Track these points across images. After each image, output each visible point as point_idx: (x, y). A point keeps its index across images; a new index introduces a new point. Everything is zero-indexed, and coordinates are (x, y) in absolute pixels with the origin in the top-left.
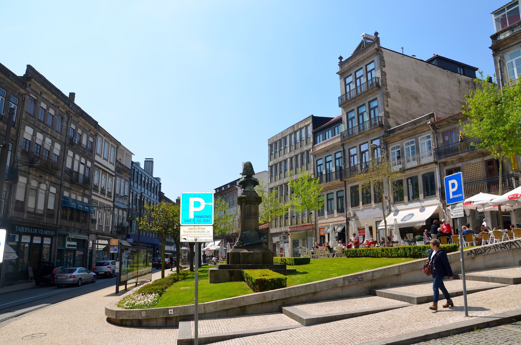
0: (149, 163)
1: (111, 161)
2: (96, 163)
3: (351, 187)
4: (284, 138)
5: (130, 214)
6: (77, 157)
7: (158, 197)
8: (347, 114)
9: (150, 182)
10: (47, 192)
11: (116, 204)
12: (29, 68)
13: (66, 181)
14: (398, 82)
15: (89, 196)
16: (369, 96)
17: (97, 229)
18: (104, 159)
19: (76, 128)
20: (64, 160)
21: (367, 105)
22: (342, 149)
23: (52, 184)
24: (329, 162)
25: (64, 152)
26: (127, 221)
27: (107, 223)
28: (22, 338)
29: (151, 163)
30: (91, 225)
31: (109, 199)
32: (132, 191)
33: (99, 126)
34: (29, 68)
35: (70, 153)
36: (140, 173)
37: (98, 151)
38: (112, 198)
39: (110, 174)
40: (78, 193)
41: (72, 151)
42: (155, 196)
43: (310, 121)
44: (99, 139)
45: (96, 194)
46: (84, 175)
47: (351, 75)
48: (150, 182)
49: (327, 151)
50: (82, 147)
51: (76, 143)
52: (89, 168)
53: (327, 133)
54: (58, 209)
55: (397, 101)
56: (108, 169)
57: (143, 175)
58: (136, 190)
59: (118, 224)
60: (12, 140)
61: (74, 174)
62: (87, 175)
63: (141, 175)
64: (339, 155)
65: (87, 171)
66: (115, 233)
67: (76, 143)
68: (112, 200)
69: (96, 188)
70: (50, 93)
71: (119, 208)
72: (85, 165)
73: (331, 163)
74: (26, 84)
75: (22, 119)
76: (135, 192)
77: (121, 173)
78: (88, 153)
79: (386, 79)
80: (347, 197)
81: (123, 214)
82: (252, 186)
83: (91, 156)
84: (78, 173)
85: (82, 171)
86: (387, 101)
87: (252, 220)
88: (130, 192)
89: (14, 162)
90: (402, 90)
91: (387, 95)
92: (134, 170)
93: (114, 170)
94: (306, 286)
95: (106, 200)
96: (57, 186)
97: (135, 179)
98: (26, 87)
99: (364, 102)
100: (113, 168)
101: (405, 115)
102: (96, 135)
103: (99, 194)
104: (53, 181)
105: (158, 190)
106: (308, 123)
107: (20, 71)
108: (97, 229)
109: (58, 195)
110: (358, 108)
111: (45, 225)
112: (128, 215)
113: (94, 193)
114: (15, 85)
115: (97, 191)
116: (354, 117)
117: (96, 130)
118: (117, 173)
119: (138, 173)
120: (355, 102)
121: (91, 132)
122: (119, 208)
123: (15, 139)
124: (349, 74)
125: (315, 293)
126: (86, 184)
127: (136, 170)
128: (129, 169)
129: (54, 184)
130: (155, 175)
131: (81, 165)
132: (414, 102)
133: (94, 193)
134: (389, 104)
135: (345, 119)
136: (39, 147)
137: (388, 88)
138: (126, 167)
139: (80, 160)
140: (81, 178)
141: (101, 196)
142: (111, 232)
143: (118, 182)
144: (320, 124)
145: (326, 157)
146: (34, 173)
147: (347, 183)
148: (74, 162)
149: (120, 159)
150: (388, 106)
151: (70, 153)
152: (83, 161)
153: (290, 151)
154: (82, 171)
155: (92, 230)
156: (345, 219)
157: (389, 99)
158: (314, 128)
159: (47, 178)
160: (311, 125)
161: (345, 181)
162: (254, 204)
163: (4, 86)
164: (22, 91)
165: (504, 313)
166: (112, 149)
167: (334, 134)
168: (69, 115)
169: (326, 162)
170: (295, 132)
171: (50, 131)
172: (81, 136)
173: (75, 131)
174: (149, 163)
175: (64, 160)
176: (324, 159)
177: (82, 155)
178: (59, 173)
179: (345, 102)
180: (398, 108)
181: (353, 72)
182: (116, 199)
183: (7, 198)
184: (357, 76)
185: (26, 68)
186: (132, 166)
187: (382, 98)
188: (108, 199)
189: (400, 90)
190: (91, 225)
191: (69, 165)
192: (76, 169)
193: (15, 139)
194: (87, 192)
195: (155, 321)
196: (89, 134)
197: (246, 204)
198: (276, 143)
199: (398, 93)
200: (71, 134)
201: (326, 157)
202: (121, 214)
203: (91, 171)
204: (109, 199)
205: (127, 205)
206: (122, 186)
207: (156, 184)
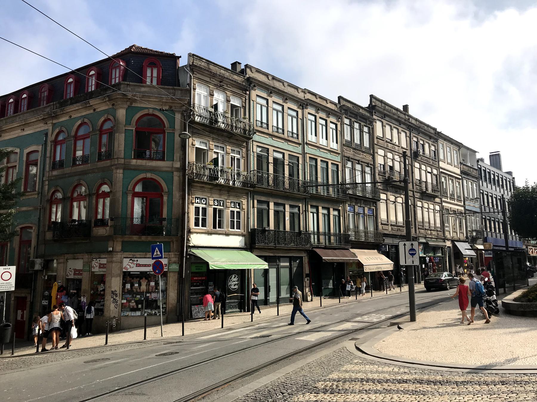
2: (441, 170)
6: (423, 167)
31: (460, 203)
38: (462, 202)
45: (446, 200)
68: (462, 204)
92: (480, 169)
95: (457, 205)
100: (458, 171)
113: (443, 199)
119: (485, 171)
127: (483, 168)
133: (443, 199)
146: (391, 188)
151: (417, 165)
152: (429, 169)
177: (427, 164)
191: (417, 177)
192: (424, 179)
193: (372, 163)
206: (470, 187)
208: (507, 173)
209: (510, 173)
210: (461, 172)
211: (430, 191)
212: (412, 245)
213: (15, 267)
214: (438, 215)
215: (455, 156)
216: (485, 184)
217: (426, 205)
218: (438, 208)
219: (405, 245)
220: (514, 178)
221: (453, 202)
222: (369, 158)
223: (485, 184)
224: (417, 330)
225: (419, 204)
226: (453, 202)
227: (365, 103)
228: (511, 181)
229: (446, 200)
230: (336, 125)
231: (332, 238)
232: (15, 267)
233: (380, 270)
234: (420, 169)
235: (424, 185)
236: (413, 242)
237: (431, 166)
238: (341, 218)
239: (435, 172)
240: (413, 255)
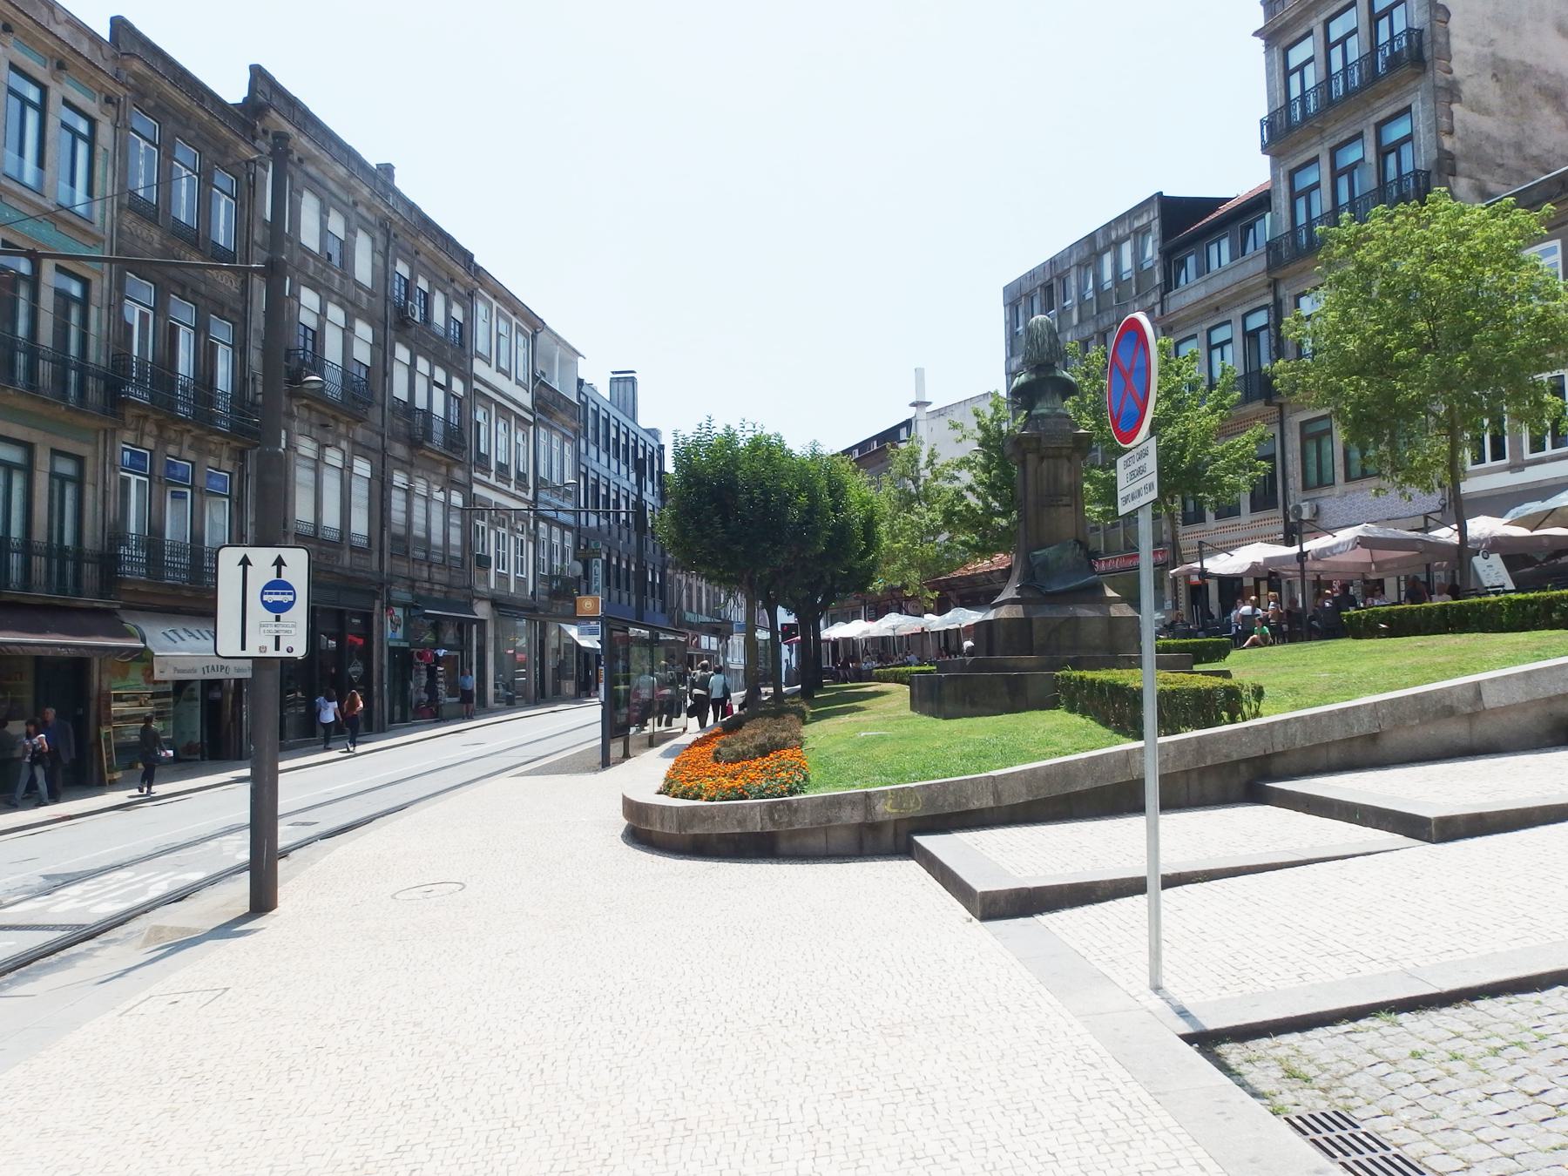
0: (625, 383)
1: (521, 377)
2: (476, 385)
3: (1303, 424)
4: (1058, 277)
5: (583, 541)
6: (423, 365)
8: (1292, 175)
9: (631, 444)
10: (346, 473)
12: (258, 75)
13: (398, 441)
14: (1491, 42)
15: (464, 486)
16: (1378, 104)
18: (499, 370)
19: (411, 274)
20: (385, 374)
21: (1370, 136)
22: (1269, 300)
23: (359, 450)
24: (1221, 345)
25: (383, 350)
26: (576, 558)
27: (519, 566)
28: (393, 897)
29: (629, 385)
30: (477, 573)
31: (523, 495)
32: (583, 469)
33: (478, 269)
34: (258, 75)
35: (402, 353)
37: (481, 345)
38: (531, 491)
39: (518, 417)
40: (433, 477)
41: (407, 346)
43: (1155, 212)
44: (481, 308)
45: (485, 478)
46: (446, 420)
47: (1310, 33)
48: (631, 444)
49: (1214, 309)
50: (435, 334)
51: (417, 318)
52: (460, 400)
53: (1214, 249)
55: (1486, 111)
56: (514, 402)
57: (613, 421)
58: (595, 465)
59: (550, 572)
60: (232, 310)
61: (419, 418)
62: (454, 420)
63: (607, 421)
64: (1258, 320)
65: (454, 411)
66: (545, 598)
67: (417, 318)
68: (530, 497)
69: (482, 462)
70: (326, 158)
71: (551, 522)
72: (446, 388)
73: (1228, 349)
74: (254, 127)
75: (255, 243)
76: (591, 475)
77: (551, 415)
78: (453, 352)
79: (1447, 34)
80: (1289, 456)
81: (563, 539)
82: (1058, 398)
83: (463, 363)
84: (428, 413)
85: (438, 409)
86: (1451, 115)
87: (1063, 510)
88: (577, 474)
89: (244, 381)
90: (1507, 71)
91: (1452, 92)
92: (586, 405)
94: (1528, 674)
95: (514, 497)
96: (374, 456)
98: (254, 138)
99: (1358, 128)
100: (526, 399)
101: (1513, 161)
102: (471, 294)
103: (492, 480)
104: (359, 439)
106: (1144, 220)
107: (233, 90)
109: (376, 484)
110: (1333, 152)
111: (349, 573)
112: (577, 543)
113: (477, 475)
114: (224, 131)
115: (486, 470)
116: (1317, 186)
117: (469, 279)
118: (538, 415)
119: (596, 413)
120: (1322, 130)
121: (456, 285)
122: (551, 522)
123: (240, 307)
124: (1302, 31)
125: (1373, 738)
126: (449, 449)
127: (592, 405)
128: (571, 403)
130: (645, 420)
132: (1547, 111)
133: (477, 475)
134: (1457, 125)
135: (1281, 201)
136: (310, 335)
137: (1454, 65)
139: (432, 375)
140: (438, 428)
141: (499, 484)
142: (533, 593)
143: (542, 440)
144: (1184, 223)
145: (1245, 317)
146: (305, 413)
147: (1287, 410)
148: (413, 380)
149: (543, 374)
150: (1451, 133)
151: (402, 353)
152: (440, 376)
153: (1080, 320)
154: (438, 409)
155: (481, 588)
156: (1281, 527)
157: (1455, 107)
158: (1166, 233)
159: (342, 429)
160: (1156, 226)
161: (1281, 406)
162: (1069, 460)
163: (192, 133)
164: (245, 150)
166: (521, 338)
167: (1239, 251)
168: (388, 231)
169: (1211, 348)
170: (1098, 256)
171: (337, 282)
172: (427, 299)
173: (408, 285)
174: (625, 383)
175: (387, 374)
176: (1202, 336)
177: (436, 359)
178: (375, 415)
179: (1281, 133)
180: (1488, 137)
181: (1316, 24)
182: (543, 495)
183: (235, 493)
184: (1334, 37)
185: (246, 76)
186: (580, 392)
187: (1430, 105)
188: (518, 493)
189: (1501, 70)
190: (477, 573)
191: (400, 390)
192: (421, 402)
193: (240, 307)
194: (459, 474)
195: (823, 837)
196: (449, 291)
197: (1042, 459)
198: (1030, 297)
199: (1491, 83)
200: (397, 290)
201: (1209, 331)
202: (556, 540)
203: (464, 405)
204: (523, 495)
206: (555, 456)
207: (649, 449)
208: (647, 431)
209: (654, 433)
212: (279, 563)
214: (455, 520)
215: (522, 352)
216: (593, 450)
217: (420, 487)
218: (457, 499)
219: (245, 562)
221: (505, 487)
222: (227, 282)
223: (593, 450)
225: (399, 479)
226: (505, 487)
227: (233, 90)
229: (485, 478)
230: (92, 123)
231: (88, 568)
234: (412, 367)
235: (419, 418)
236: (286, 553)
238: (89, 490)
239: (458, 387)
240: (278, 608)
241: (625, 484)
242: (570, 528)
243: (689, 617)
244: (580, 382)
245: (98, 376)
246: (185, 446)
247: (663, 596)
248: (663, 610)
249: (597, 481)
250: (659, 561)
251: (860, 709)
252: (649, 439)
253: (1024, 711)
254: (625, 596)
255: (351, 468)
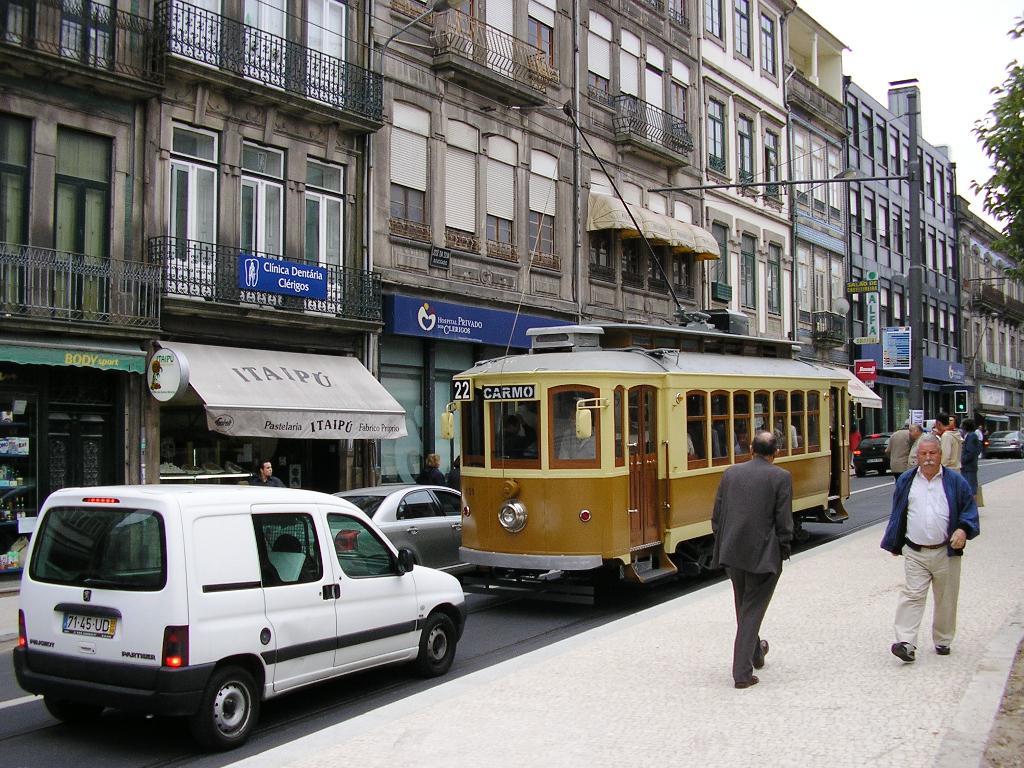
2: (705, 72)
6: (629, 42)
7: (948, 216)
11: (804, 233)
17: (762, 330)
19: (890, 285)
35: (599, 25)
36: (876, 121)
42: (939, 210)
54: (576, 247)
61: (625, 106)
62: (677, 111)
68: (785, 215)
71: (809, 245)
72: (664, 73)
84: (638, 101)
92: (855, 109)
93: (780, 103)
95: (761, 214)
96: (560, 151)
97: (864, 145)
100: (776, 95)
105: (947, 189)
108: (762, 330)
119: (870, 120)
128: (835, 103)
129: (548, 146)
131: (649, 74)
138: (823, 95)
152: (655, 58)
165: (153, 195)
174: (908, 94)
183: (351, 190)
186: (846, 93)
205: (843, 239)
210: (788, 102)
211: (654, 135)
213: (729, 582)
220: (953, 166)
221: (749, 201)
224: (486, 654)
226: (775, 212)
228: (946, 174)
232: (729, 582)
233: (158, 446)
234: (615, 42)
237: (663, 45)
241: (940, 227)
242: (839, 256)
243: (992, 368)
244: (847, 80)
245: (132, 28)
246: (269, 128)
247: (958, 343)
248: (959, 358)
249: (900, 217)
250: (952, 300)
251: (85, 500)
252: (937, 156)
253: (997, 478)
254: (943, 351)
255: (527, 166)
